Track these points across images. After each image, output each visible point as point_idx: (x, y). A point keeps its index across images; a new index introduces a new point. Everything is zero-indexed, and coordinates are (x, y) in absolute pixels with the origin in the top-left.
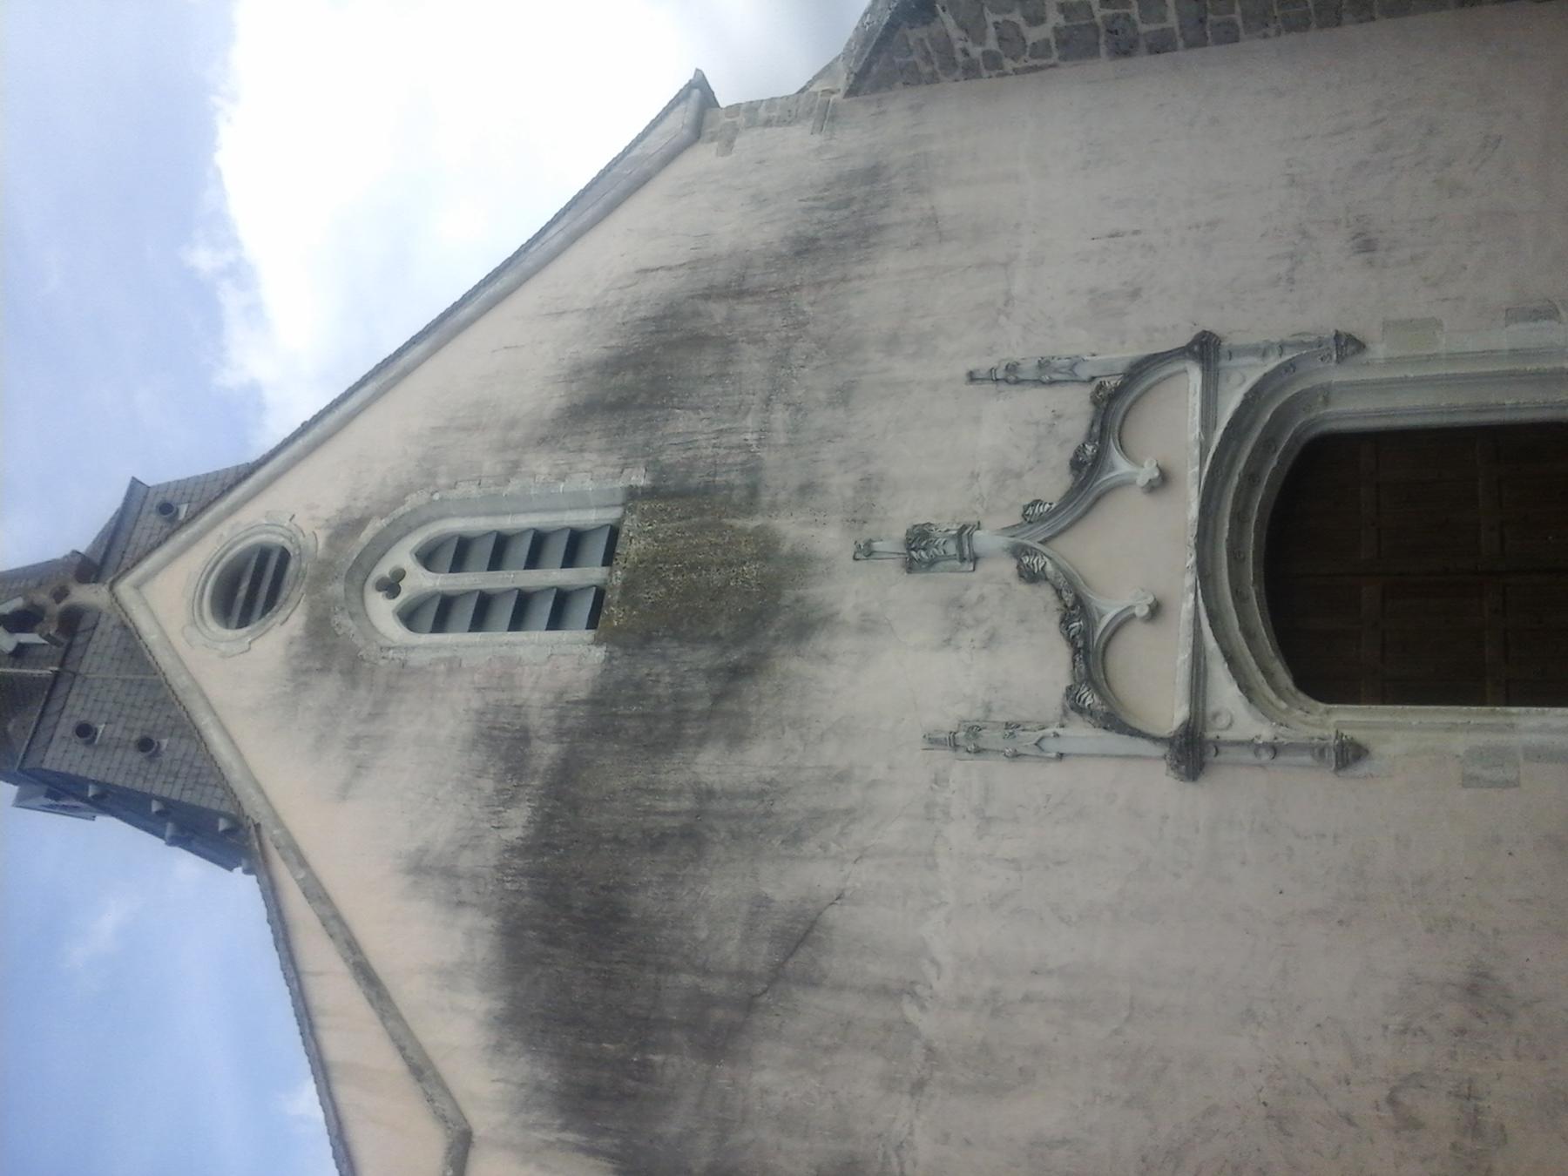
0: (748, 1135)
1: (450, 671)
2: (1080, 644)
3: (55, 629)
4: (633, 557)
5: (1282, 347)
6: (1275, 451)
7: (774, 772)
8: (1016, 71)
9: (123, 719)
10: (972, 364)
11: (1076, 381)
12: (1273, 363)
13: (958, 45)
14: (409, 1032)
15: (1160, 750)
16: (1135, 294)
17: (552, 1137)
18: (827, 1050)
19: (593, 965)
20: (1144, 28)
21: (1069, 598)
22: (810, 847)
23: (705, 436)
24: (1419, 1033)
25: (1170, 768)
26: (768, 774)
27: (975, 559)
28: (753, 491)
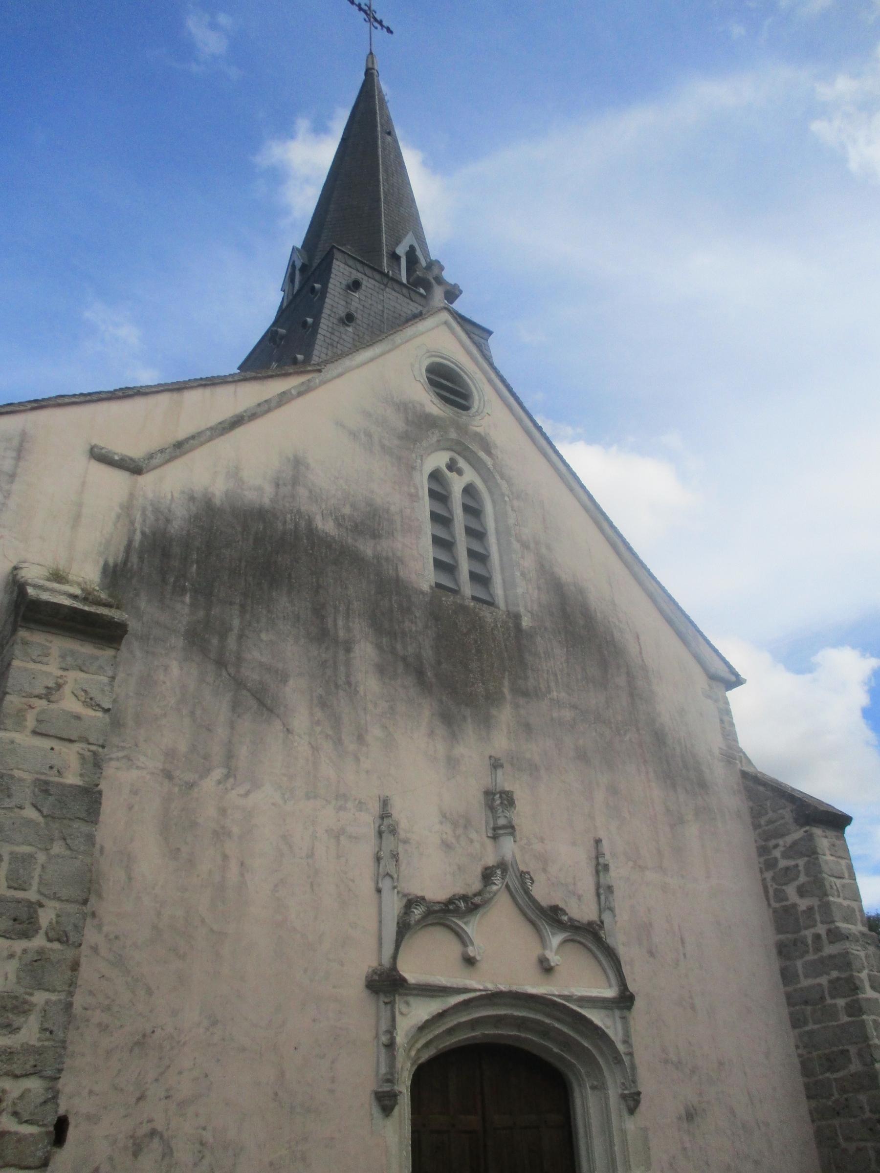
0: (138, 654)
1: (411, 495)
2: (451, 907)
3: (420, 275)
4: (482, 614)
5: (631, 1054)
6: (562, 1051)
7: (362, 693)
8: (764, 880)
9: (361, 307)
10: (605, 843)
11: (600, 911)
12: (621, 1047)
13: (781, 842)
14: (202, 444)
15: (386, 961)
16: (651, 953)
17: (137, 526)
18: (192, 713)
19: (243, 564)
21: (477, 900)
22: (319, 714)
23: (553, 666)
24: (201, 1156)
25: (374, 968)
26: (361, 689)
27: (495, 838)
28: (526, 694)
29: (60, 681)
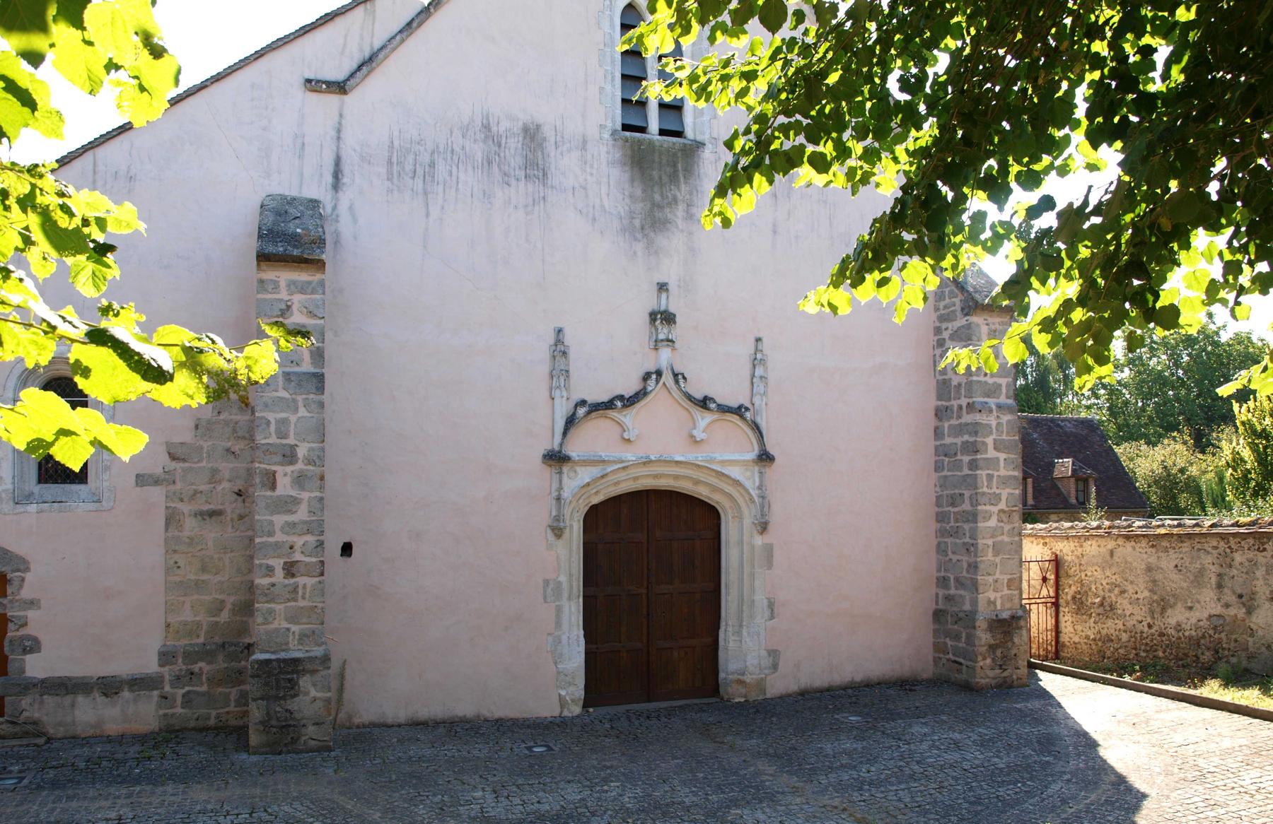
13: (950, 325)
20: (946, 425)
29: (289, 303)
